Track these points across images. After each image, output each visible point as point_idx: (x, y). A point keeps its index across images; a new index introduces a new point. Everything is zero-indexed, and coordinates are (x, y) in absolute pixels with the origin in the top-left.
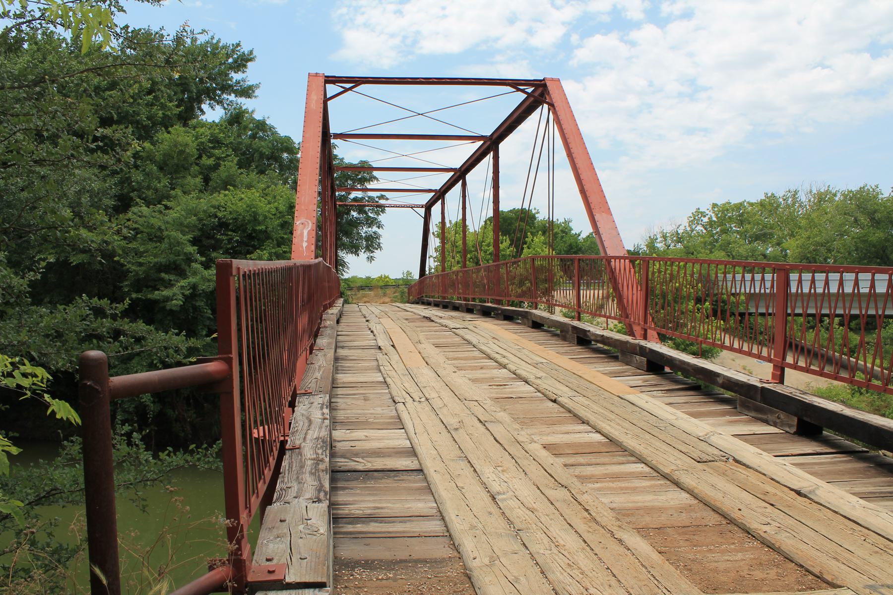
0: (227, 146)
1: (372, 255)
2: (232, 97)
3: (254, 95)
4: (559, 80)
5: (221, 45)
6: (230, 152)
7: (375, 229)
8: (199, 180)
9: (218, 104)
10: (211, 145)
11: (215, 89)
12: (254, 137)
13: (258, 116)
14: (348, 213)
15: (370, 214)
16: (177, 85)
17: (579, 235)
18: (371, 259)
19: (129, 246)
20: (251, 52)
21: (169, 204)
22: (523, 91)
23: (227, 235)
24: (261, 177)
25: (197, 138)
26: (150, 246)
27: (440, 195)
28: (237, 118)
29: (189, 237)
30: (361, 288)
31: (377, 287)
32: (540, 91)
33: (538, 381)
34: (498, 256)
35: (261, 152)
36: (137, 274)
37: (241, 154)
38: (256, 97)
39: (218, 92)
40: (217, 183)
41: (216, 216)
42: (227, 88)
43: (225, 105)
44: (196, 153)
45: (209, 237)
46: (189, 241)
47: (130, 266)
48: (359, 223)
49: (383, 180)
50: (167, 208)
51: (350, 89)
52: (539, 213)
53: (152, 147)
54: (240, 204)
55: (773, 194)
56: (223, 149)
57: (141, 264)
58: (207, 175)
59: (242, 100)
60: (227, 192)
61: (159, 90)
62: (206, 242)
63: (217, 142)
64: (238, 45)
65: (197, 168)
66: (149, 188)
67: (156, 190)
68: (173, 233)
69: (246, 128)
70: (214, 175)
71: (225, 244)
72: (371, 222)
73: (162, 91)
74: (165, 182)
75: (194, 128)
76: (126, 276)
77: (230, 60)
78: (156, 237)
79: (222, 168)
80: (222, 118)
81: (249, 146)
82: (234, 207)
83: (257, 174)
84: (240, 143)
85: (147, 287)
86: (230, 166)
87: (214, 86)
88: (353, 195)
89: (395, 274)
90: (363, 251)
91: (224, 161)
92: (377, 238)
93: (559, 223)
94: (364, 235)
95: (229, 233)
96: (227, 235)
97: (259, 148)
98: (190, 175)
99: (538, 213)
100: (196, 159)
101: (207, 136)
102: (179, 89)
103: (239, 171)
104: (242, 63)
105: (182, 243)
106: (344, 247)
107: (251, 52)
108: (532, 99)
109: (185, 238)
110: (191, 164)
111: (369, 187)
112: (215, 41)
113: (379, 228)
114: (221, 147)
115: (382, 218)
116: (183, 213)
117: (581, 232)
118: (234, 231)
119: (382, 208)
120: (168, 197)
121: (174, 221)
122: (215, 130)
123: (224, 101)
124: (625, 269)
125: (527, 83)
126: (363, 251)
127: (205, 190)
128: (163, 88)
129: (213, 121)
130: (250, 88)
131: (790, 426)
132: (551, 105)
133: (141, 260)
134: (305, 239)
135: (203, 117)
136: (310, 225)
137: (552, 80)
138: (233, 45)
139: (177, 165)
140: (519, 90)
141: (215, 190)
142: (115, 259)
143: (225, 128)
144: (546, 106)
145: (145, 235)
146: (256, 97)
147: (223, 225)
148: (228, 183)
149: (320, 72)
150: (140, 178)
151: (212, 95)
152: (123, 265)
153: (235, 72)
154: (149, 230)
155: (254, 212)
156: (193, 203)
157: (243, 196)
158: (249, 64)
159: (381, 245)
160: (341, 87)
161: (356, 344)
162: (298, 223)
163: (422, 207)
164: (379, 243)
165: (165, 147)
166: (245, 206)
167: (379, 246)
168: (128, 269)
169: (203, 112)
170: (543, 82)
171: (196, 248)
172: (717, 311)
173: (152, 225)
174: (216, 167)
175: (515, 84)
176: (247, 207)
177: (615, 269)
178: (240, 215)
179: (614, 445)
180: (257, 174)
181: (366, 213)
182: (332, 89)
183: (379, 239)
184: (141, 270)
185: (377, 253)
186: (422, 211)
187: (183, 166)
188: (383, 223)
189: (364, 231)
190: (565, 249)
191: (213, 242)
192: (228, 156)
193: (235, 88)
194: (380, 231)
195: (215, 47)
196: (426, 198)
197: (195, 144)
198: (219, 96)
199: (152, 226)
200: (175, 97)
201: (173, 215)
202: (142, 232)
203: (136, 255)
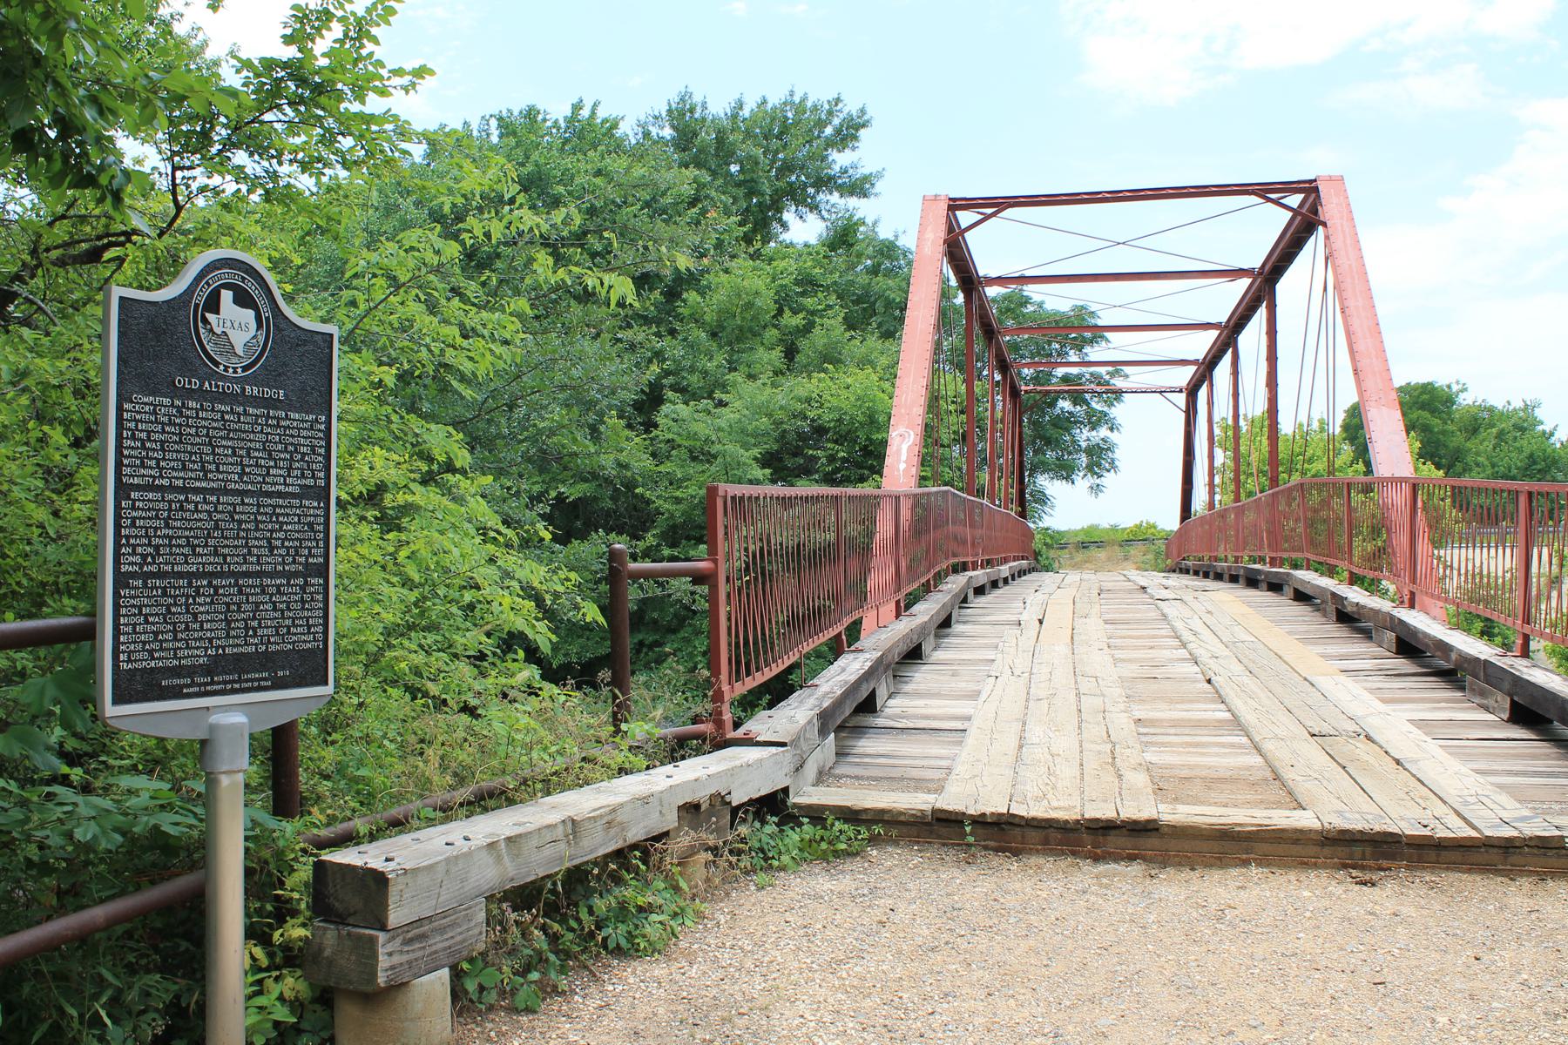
0: (828, 288)
1: (1098, 481)
2: (835, 198)
3: (874, 191)
4: (1341, 179)
5: (809, 104)
6: (833, 299)
7: (1103, 432)
8: (777, 354)
9: (811, 211)
10: (799, 290)
11: (805, 186)
12: (874, 271)
13: (884, 233)
14: (1053, 404)
15: (1094, 405)
16: (739, 185)
17: (1552, 434)
18: (1096, 489)
19: (661, 468)
20: (863, 111)
21: (724, 397)
23: (825, 449)
24: (887, 344)
25: (774, 280)
26: (693, 469)
27: (1207, 368)
28: (843, 237)
29: (756, 452)
30: (1084, 546)
31: (1112, 543)
33: (1212, 663)
34: (1277, 481)
35: (887, 298)
36: (672, 516)
37: (853, 301)
38: (876, 195)
39: (811, 191)
40: (809, 356)
41: (806, 418)
42: (825, 182)
43: (823, 212)
44: (774, 307)
45: (797, 453)
46: (755, 459)
47: (661, 502)
48: (1075, 422)
49: (1117, 347)
50: (722, 404)
52: (1466, 390)
53: (699, 299)
54: (844, 394)
56: (820, 294)
57: (678, 501)
58: (793, 343)
59: (853, 202)
60: (823, 375)
61: (707, 197)
62: (790, 462)
63: (808, 284)
64: (838, 101)
65: (775, 332)
66: (692, 370)
67: (705, 373)
68: (730, 447)
69: (859, 255)
70: (803, 344)
71: (823, 464)
72: (1095, 420)
73: (712, 199)
74: (720, 358)
75: (771, 260)
76: (654, 522)
77: (829, 131)
78: (701, 455)
79: (817, 330)
80: (820, 236)
81: (867, 288)
82: (835, 402)
83: (880, 338)
84: (852, 283)
85: (688, 538)
86: (831, 327)
87: (803, 178)
88: (1060, 371)
89: (1127, 519)
90: (1081, 474)
91: (822, 317)
92: (1109, 449)
93: (1511, 408)
94: (1084, 445)
95: (829, 445)
96: (825, 449)
97: (885, 291)
98: (763, 344)
99: (1464, 390)
100: (774, 317)
101: (792, 274)
102: (741, 192)
103: (848, 335)
104: (848, 134)
105: (744, 464)
106: (1043, 467)
107: (863, 111)
109: (747, 456)
110: (765, 327)
111: (1093, 357)
112: (797, 99)
113: (1112, 429)
114: (816, 292)
115: (1117, 412)
116: (745, 412)
117: (1555, 429)
118: (836, 442)
119: (1118, 393)
120: (724, 387)
121: (730, 426)
122: (805, 262)
123: (822, 206)
125: (1289, 187)
126: (1081, 474)
127: (788, 369)
128: (713, 194)
130: (866, 179)
131: (1503, 710)
133: (678, 494)
134: (904, 457)
135: (786, 237)
136: (912, 437)
137: (1330, 179)
138: (829, 102)
139: (741, 329)
141: (807, 370)
142: (637, 491)
143: (825, 257)
144: (1320, 228)
145: (684, 450)
146: (876, 195)
147: (820, 431)
148: (830, 358)
150: (679, 352)
151: (798, 196)
152: (648, 502)
153: (839, 151)
154: (691, 443)
155: (868, 408)
156: (764, 395)
157: (849, 381)
158: (862, 132)
159: (1117, 463)
161: (988, 618)
162: (894, 434)
163: (1181, 391)
164: (1113, 460)
165: (719, 297)
166: (852, 399)
167: (1113, 466)
168: (657, 509)
169: (784, 226)
171: (768, 471)
173: (696, 434)
174: (807, 329)
175: (1264, 191)
176: (857, 400)
178: (845, 413)
179: (1237, 724)
180: (880, 338)
181: (1088, 404)
182: (965, 218)
183: (1113, 452)
184: (678, 511)
185: (1109, 479)
186: (1181, 399)
187: (751, 330)
188: (1119, 421)
189: (1084, 436)
190: (1519, 464)
191: (802, 461)
192: (830, 307)
193: (840, 181)
194: (1114, 437)
195: (800, 108)
196: (1185, 375)
197: (772, 293)
198: (813, 197)
199: (694, 436)
200: (734, 208)
201: (727, 416)
202: (679, 446)
203: (671, 484)
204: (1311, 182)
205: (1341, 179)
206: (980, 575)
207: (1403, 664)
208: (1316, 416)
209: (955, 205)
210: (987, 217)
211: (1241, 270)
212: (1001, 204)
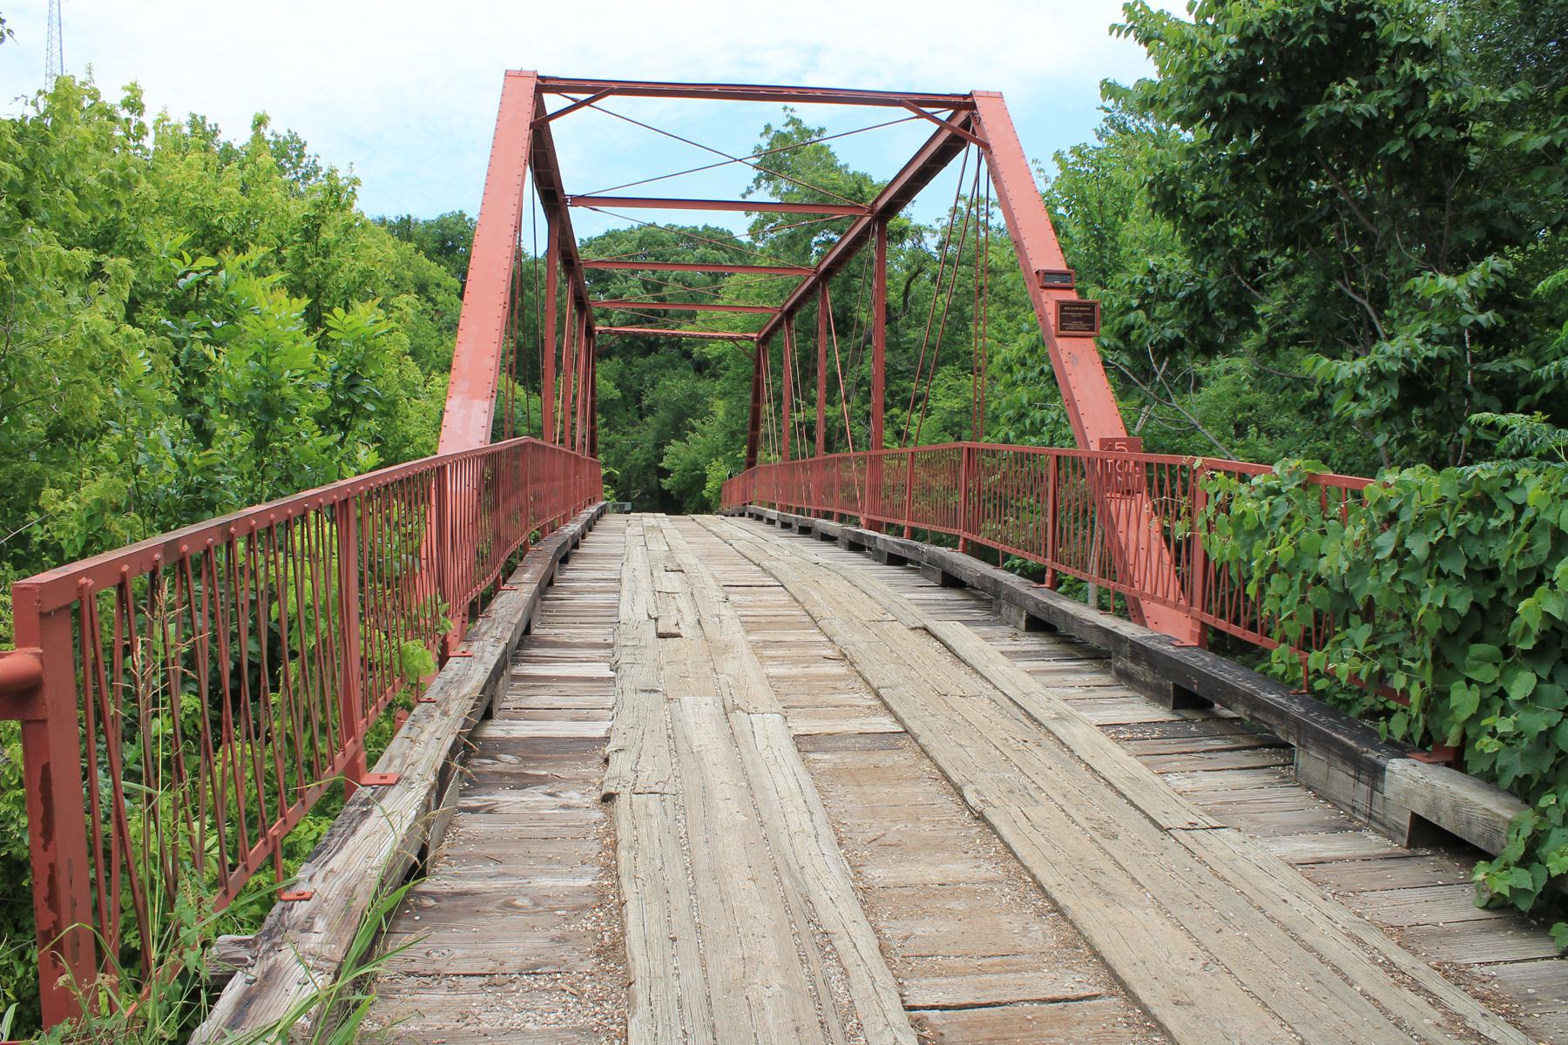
4: (1000, 96)
22: (931, 117)
32: (963, 115)
51: (587, 102)
55: (196, 123)
108: (946, 134)
124: (1137, 549)
129: (203, 118)
132: (985, 146)
137: (988, 95)
140: (922, 115)
144: (973, 147)
149: (529, 67)
160: (573, 99)
170: (969, 100)
172: (996, 564)
175: (918, 103)
177: (1127, 545)
182: (553, 102)
204: (965, 97)
205: (1000, 96)
206: (550, 546)
207: (1033, 643)
208: (587, 599)
209: (545, 85)
210: (578, 105)
211: (583, 196)
212: (598, 90)
